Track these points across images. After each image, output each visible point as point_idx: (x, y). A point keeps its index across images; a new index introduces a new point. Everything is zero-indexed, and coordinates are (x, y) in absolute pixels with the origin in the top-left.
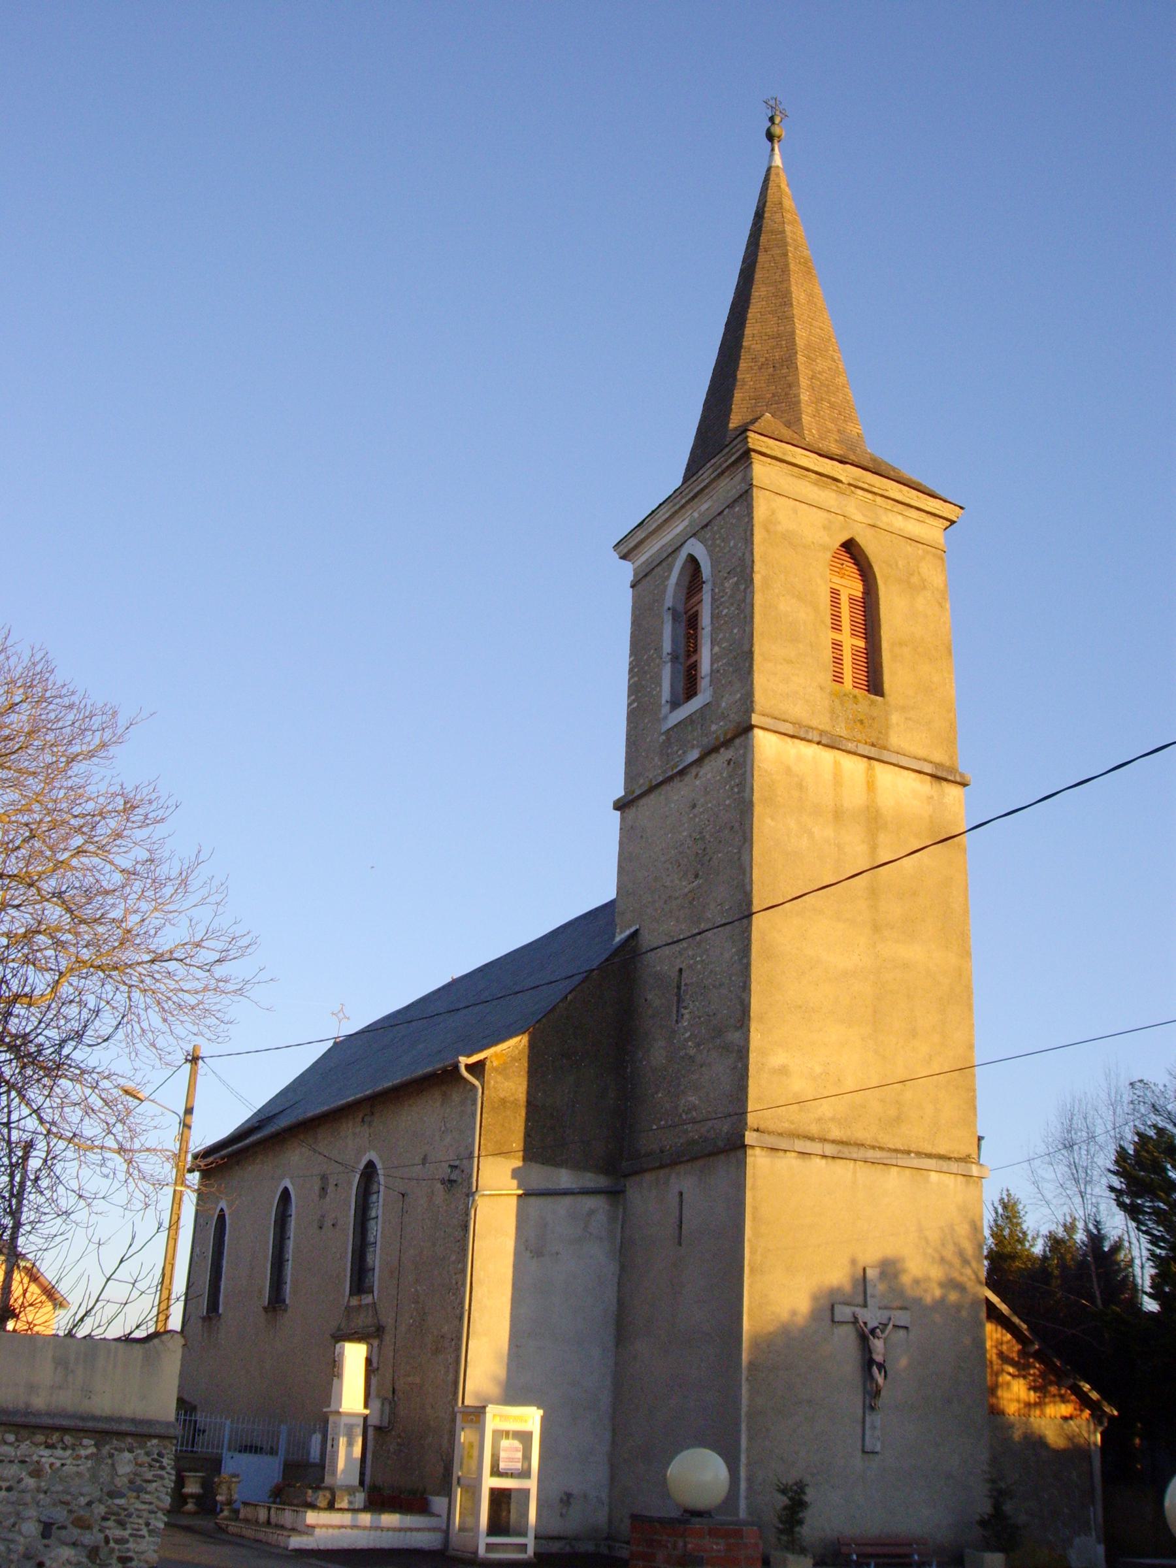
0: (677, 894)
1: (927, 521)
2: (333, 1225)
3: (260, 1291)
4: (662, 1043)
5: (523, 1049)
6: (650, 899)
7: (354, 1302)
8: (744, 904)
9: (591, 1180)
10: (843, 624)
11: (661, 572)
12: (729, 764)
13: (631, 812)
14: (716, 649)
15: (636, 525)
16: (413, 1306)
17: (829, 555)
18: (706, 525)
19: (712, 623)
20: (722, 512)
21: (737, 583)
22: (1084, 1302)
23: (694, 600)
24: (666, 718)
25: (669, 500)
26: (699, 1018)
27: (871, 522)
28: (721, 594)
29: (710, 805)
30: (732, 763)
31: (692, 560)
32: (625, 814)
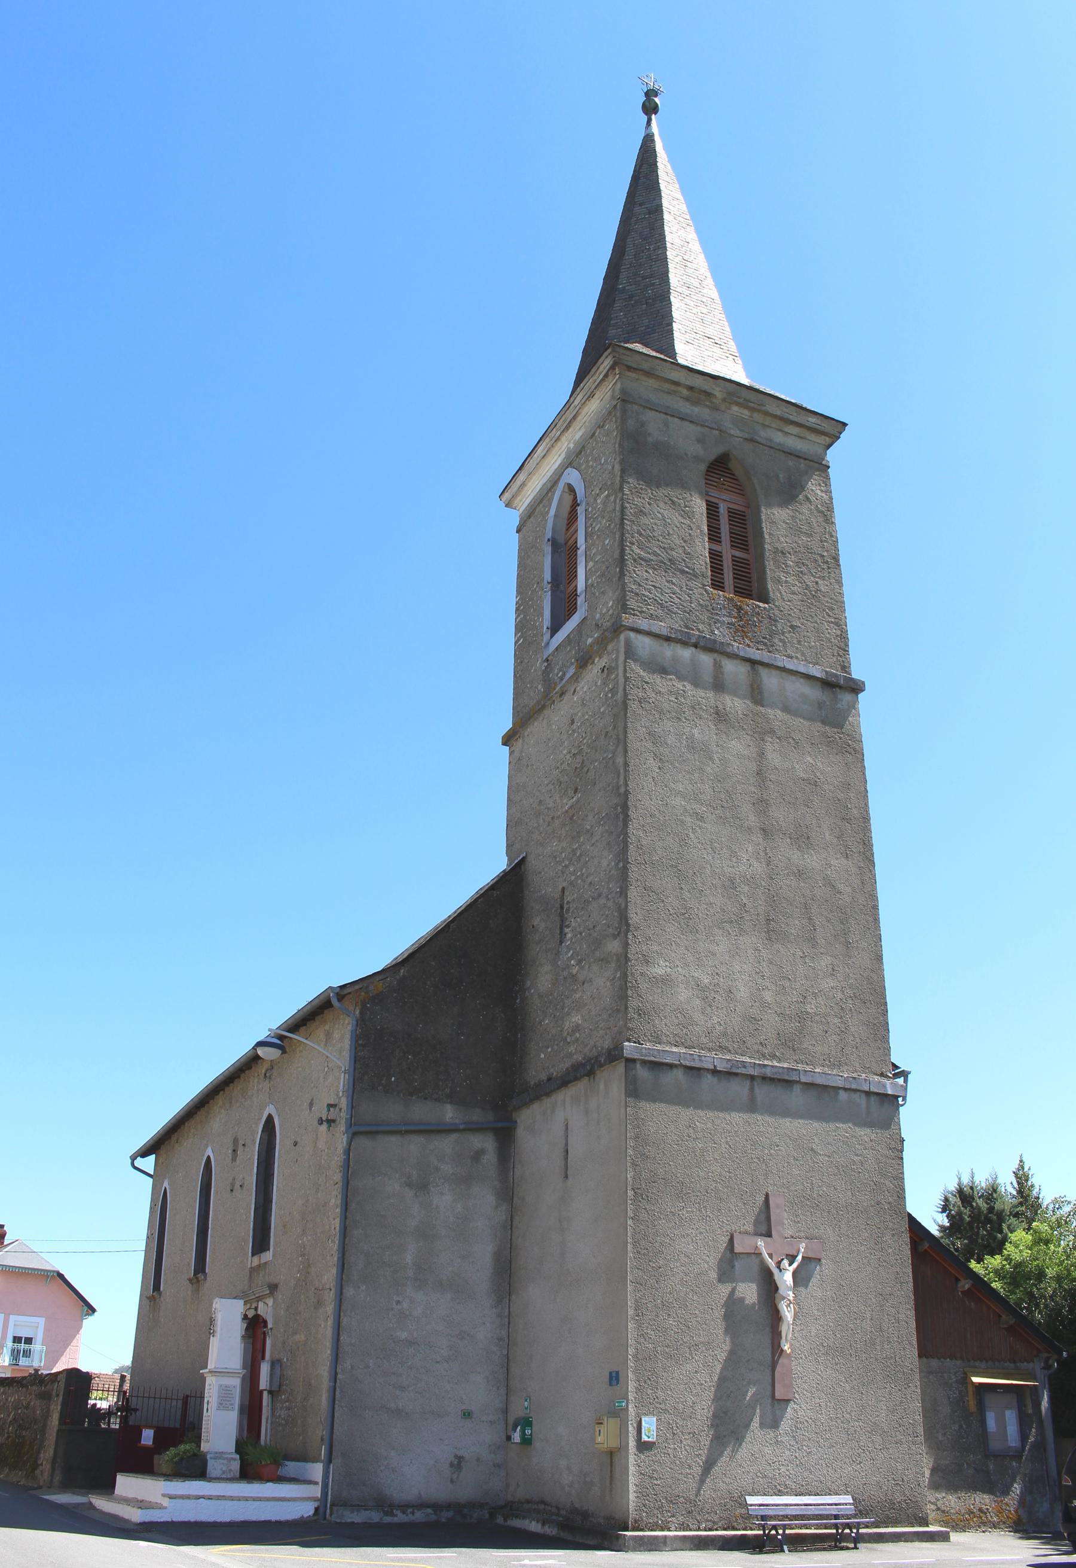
0: (559, 813)
1: (809, 438)
2: (241, 1186)
3: (189, 1264)
4: (547, 967)
5: (762, 1204)
6: (535, 825)
7: (256, 1261)
8: (619, 808)
9: (477, 1116)
10: (723, 535)
11: (542, 509)
12: (603, 671)
13: (518, 745)
14: (591, 564)
15: (518, 468)
16: (300, 1259)
17: (703, 467)
18: (580, 452)
19: (586, 541)
20: (594, 434)
21: (608, 496)
22: (1056, 1364)
23: (572, 530)
24: (548, 644)
25: (546, 435)
26: (581, 934)
27: (747, 436)
28: (594, 512)
29: (587, 717)
30: (605, 669)
31: (571, 489)
32: (512, 749)
